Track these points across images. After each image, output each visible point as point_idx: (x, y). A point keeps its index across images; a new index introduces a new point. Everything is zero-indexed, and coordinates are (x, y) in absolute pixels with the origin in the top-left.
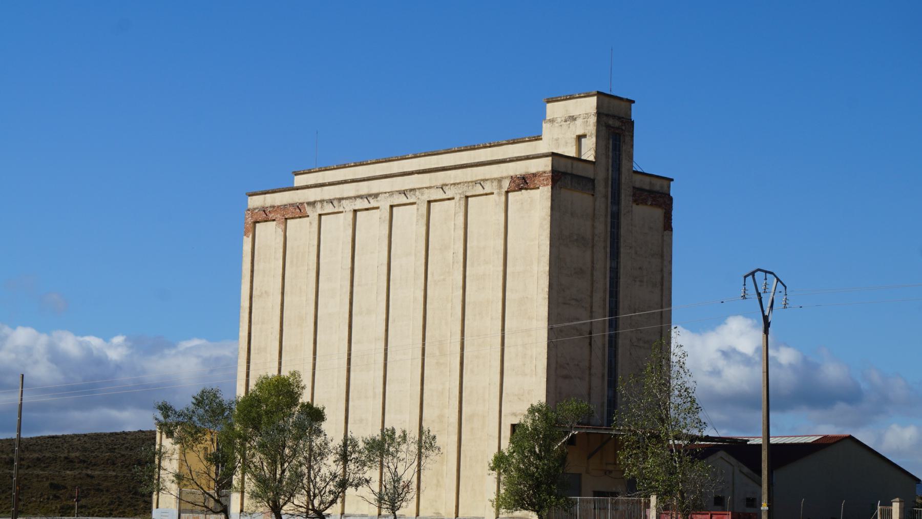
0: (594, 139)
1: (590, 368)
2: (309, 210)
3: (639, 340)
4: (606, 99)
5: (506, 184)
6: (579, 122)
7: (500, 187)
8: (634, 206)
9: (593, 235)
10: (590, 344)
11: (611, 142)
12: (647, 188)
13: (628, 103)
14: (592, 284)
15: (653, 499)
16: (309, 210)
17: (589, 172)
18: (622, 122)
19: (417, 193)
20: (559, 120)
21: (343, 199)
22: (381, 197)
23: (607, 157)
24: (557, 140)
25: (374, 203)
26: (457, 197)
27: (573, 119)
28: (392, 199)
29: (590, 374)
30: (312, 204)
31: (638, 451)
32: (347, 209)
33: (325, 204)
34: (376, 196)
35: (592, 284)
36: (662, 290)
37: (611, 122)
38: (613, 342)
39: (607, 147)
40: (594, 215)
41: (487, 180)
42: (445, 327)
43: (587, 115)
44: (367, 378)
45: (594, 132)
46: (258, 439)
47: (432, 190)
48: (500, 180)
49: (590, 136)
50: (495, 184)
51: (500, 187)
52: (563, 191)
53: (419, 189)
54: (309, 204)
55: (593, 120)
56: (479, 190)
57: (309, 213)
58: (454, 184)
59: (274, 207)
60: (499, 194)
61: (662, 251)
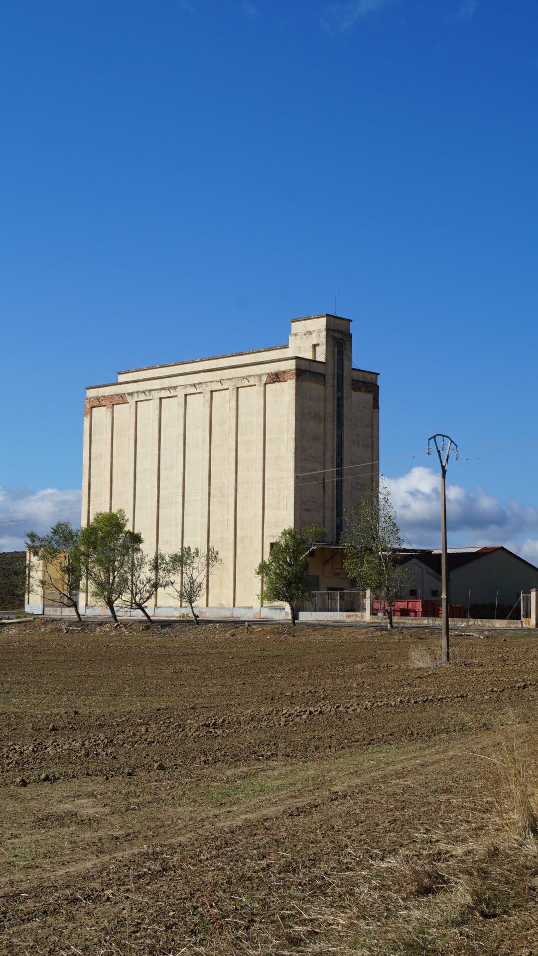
0: (324, 347)
2: (129, 398)
4: (333, 319)
5: (264, 379)
6: (314, 335)
12: (362, 380)
14: (325, 446)
16: (129, 398)
17: (322, 370)
27: (310, 333)
30: (131, 394)
34: (175, 388)
37: (336, 335)
38: (339, 486)
39: (334, 353)
43: (319, 331)
45: (324, 342)
48: (260, 376)
51: (261, 381)
54: (128, 394)
55: (324, 333)
56: (246, 383)
60: (260, 385)
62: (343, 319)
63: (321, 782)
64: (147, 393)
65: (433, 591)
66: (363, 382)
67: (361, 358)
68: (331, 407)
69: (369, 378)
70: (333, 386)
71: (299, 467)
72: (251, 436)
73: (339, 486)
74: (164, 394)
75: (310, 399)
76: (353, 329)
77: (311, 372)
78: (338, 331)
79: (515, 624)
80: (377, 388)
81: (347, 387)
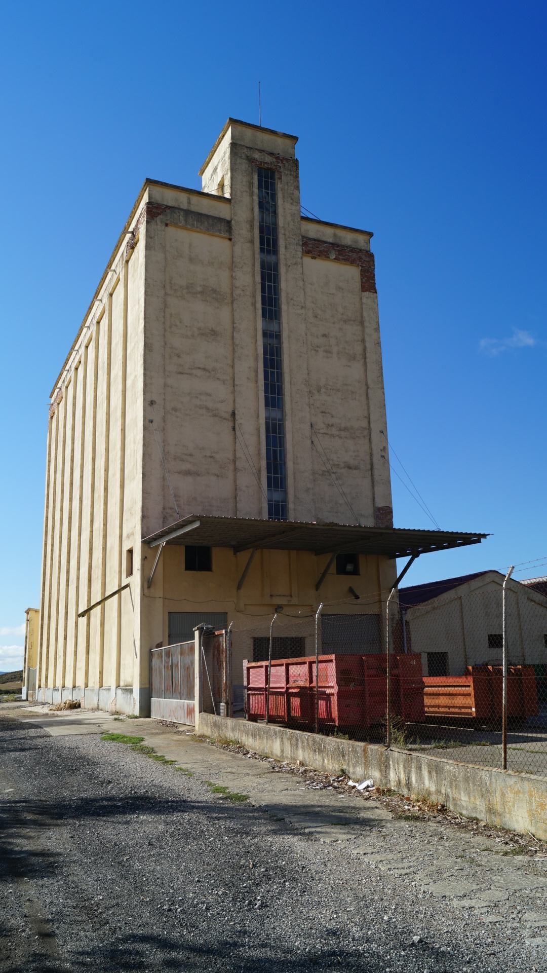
1: (234, 461)
3: (329, 426)
4: (249, 132)
8: (307, 260)
9: (233, 287)
10: (234, 429)
11: (256, 177)
12: (331, 240)
13: (288, 142)
14: (234, 351)
15: (197, 633)
17: (223, 211)
18: (278, 158)
23: (252, 194)
29: (235, 469)
35: (234, 351)
36: (365, 364)
37: (257, 156)
38: (275, 434)
39: (251, 184)
40: (233, 262)
46: (257, 679)
52: (171, 230)
61: (362, 317)
62: (273, 132)
65: (191, 565)
66: (333, 245)
67: (320, 195)
68: (248, 279)
69: (280, 145)
70: (252, 242)
73: (275, 434)
75: (191, 260)
76: (300, 152)
77: (188, 212)
78: (271, 154)
79: (425, 669)
80: (296, 162)
81: (288, 251)
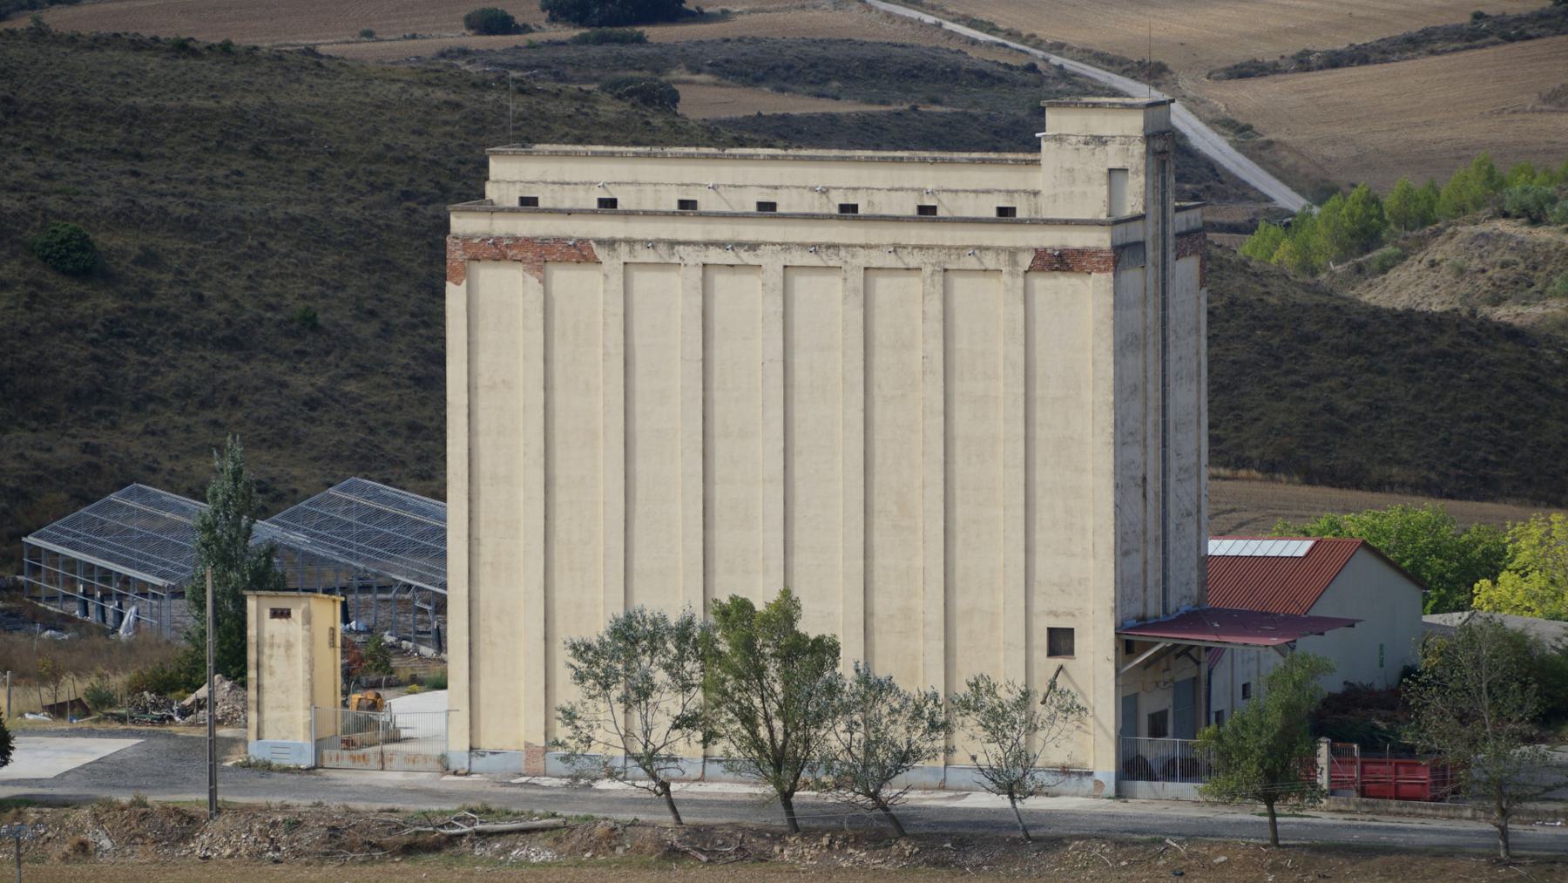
0: (1142, 179)
2: (600, 253)
5: (1026, 260)
6: (1112, 148)
7: (1014, 263)
16: (600, 253)
19: (843, 253)
20: (1074, 140)
21: (679, 243)
22: (762, 250)
24: (1070, 171)
25: (747, 257)
26: (928, 270)
27: (1101, 141)
28: (788, 257)
30: (611, 244)
31: (814, 699)
32: (690, 261)
33: (638, 247)
34: (753, 247)
41: (987, 248)
42: (912, 473)
43: (1127, 139)
44: (911, 561)
45: (1142, 167)
47: (874, 253)
48: (1013, 253)
49: (1136, 173)
50: (1003, 257)
51: (1014, 263)
53: (847, 246)
54: (600, 242)
55: (1139, 149)
56: (971, 263)
57: (600, 258)
58: (921, 248)
59: (517, 239)
60: (1012, 274)
63: (313, 544)
64: (662, 249)
71: (443, 315)
72: (992, 418)
74: (799, 258)
